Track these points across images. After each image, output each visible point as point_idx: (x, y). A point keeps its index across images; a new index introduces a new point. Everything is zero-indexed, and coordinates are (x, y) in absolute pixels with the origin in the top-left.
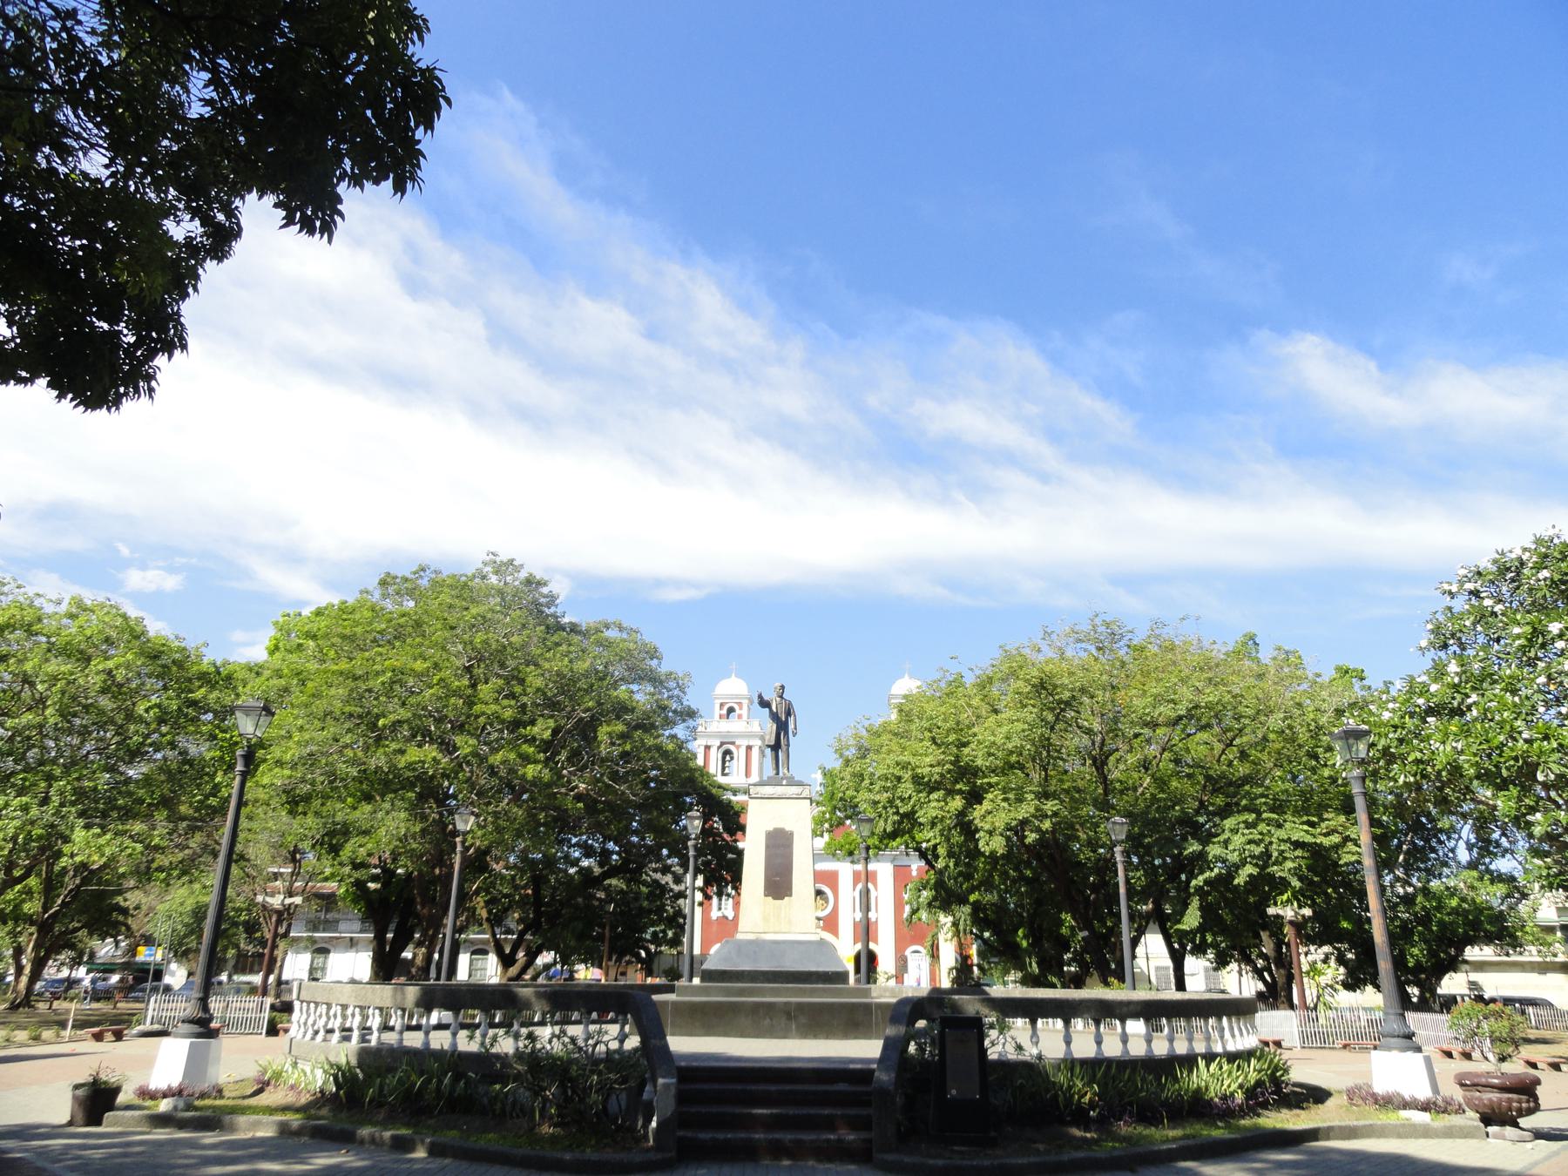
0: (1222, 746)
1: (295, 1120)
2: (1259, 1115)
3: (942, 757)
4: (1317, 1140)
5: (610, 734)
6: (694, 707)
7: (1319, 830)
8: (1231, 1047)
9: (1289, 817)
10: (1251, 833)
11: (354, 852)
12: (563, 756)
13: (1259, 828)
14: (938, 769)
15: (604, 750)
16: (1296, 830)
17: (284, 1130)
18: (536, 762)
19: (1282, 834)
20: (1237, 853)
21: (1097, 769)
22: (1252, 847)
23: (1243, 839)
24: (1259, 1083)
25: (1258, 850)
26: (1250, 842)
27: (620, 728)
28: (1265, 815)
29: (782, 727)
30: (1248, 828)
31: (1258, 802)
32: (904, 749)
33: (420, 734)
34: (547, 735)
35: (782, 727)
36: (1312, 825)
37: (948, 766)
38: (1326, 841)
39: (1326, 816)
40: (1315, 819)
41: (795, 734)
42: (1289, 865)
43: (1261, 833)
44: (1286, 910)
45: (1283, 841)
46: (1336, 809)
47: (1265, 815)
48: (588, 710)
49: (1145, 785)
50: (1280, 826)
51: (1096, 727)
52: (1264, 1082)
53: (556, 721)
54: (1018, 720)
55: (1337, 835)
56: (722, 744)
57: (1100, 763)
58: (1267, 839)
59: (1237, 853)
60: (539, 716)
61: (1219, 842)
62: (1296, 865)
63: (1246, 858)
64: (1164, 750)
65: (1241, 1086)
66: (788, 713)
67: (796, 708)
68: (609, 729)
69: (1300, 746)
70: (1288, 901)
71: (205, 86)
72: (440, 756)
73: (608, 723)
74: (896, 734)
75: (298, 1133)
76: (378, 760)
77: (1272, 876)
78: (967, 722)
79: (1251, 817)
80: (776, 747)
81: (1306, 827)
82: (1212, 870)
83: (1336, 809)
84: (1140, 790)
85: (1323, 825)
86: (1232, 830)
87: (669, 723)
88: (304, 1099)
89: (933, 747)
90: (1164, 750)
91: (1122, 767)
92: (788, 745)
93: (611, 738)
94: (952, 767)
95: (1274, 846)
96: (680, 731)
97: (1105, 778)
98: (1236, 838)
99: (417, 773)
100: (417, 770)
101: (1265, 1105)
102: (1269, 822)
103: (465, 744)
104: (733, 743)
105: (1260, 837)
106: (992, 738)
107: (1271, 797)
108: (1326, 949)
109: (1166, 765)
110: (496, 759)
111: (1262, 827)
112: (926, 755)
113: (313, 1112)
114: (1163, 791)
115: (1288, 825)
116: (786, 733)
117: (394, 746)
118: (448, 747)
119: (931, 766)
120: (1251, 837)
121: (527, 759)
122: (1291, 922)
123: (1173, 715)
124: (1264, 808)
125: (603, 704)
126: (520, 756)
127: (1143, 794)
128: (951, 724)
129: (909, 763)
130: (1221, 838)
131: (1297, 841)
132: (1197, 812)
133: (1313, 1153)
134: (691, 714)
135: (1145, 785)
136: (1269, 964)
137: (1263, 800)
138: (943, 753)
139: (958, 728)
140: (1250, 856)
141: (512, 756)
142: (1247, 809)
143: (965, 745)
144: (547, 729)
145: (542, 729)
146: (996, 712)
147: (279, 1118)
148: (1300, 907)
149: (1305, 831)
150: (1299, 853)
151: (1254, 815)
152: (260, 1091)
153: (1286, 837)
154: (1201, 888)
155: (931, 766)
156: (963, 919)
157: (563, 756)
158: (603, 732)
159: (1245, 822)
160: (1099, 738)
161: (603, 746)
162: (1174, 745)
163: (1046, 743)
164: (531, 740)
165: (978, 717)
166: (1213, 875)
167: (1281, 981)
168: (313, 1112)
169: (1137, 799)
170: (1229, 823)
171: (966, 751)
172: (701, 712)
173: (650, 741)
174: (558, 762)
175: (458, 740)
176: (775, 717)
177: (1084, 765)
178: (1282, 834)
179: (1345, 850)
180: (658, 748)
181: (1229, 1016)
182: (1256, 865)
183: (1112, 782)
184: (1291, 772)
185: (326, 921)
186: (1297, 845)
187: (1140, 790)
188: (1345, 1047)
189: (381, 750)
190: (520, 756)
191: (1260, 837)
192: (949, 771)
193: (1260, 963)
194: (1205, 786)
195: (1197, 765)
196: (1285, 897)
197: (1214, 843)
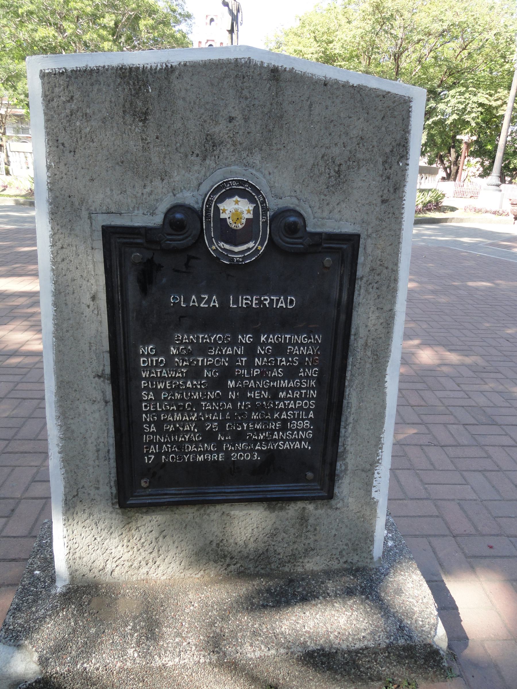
0: (460, 50)
1: (22, 200)
2: (426, 214)
3: (319, 48)
4: (446, 222)
5: (145, 25)
6: (190, 12)
7: (493, 98)
8: (423, 187)
9: (481, 90)
10: (461, 98)
11: (23, 88)
12: (123, 39)
13: (465, 96)
14: (315, 56)
15: (144, 35)
16: (482, 97)
17: (17, 203)
18: (109, 40)
19: (475, 99)
20: (451, 108)
21: (395, 61)
22: (459, 105)
23: (456, 101)
24: (430, 202)
25: (461, 107)
26: (459, 103)
27: (151, 22)
28: (470, 89)
29: (235, 19)
30: (460, 95)
31: (469, 81)
32: (300, 43)
33: (44, 21)
34: (112, 24)
35: (235, 19)
36: (491, 95)
37: (321, 54)
38: (494, 104)
39: (499, 90)
40: (493, 92)
41: (241, 24)
42: (473, 115)
43: (465, 98)
44: (465, 137)
45: (475, 103)
46: (505, 87)
47: (470, 89)
48: (133, 10)
49: (417, 71)
50: (475, 95)
51: (400, 35)
52: (432, 201)
53: (116, 17)
54: (361, 28)
55: (500, 101)
56: (208, 41)
57: (397, 57)
58: (467, 101)
59: (451, 108)
60: (107, 12)
61: (444, 102)
62: (476, 115)
63: (454, 111)
64: (431, 51)
65: (422, 202)
66: (238, 11)
67: (243, 8)
68: (145, 23)
69: (499, 51)
70: (468, 133)
71: (319, 599)
72: (56, 34)
73: (145, 19)
74: (296, 34)
75: (23, 204)
76: (23, 35)
77: (464, 120)
78: (334, 28)
79: (463, 89)
80: (231, 31)
81: (487, 96)
82: (437, 116)
83: (505, 87)
84: (414, 73)
85: (496, 95)
86: (452, 96)
87: (178, 22)
88: (24, 193)
89: (315, 42)
90: (431, 51)
91: (408, 61)
92: (238, 31)
93: (147, 28)
94: (323, 55)
95: (470, 105)
96: (183, 27)
97: (398, 67)
98: (453, 100)
99: (46, 44)
100: (46, 42)
101: (429, 210)
102: (471, 92)
103: (69, 27)
104: (213, 41)
105: (464, 100)
106: (346, 38)
107: (476, 79)
108: (478, 159)
109: (429, 60)
110: (87, 37)
111: (467, 95)
112: (310, 47)
113: (28, 197)
114: (425, 74)
115: (479, 95)
116: (237, 23)
117: (30, 27)
118: (61, 30)
119: (312, 53)
120: (460, 100)
121: (103, 39)
122: (466, 143)
123: (441, 29)
124: (471, 85)
125: (140, 6)
126: (99, 36)
127: (415, 75)
128: (325, 29)
129: (301, 51)
130: (446, 100)
131: (481, 103)
132: (439, 86)
133: (443, 226)
134: (188, 16)
135: (417, 71)
136: (451, 165)
137: (472, 80)
138: (319, 46)
139: (328, 32)
140: (457, 110)
141: (95, 36)
142: (463, 85)
143: (331, 42)
144: (111, 20)
145: (109, 20)
146: (349, 22)
147: (15, 198)
148: (472, 136)
149: (487, 98)
150: (480, 109)
151: (465, 89)
152: (4, 190)
153: (476, 101)
154: (430, 125)
155: (312, 53)
156: (361, 297)
157: (123, 39)
158: (142, 23)
159: (460, 92)
160: (399, 42)
161: (143, 33)
162: (437, 48)
163: (373, 44)
164: (105, 27)
165: (340, 25)
166: (437, 119)
167: (454, 171)
168: (28, 197)
169: (411, 78)
170: (452, 92)
171: (331, 45)
172: (194, 16)
173: (168, 32)
174: (120, 43)
175: (65, 24)
176: (231, 12)
177: (390, 58)
178: (475, 99)
179: (502, 109)
180: (172, 36)
181: (425, 174)
182: (458, 114)
183: (401, 69)
184: (490, 68)
185: (23, 129)
186: (481, 105)
187: (414, 73)
188: (471, 197)
189: (24, 29)
190: (99, 36)
191: (464, 100)
192: (321, 57)
193: (447, 164)
194: (446, 72)
195: (446, 60)
196: (466, 131)
197: (442, 103)
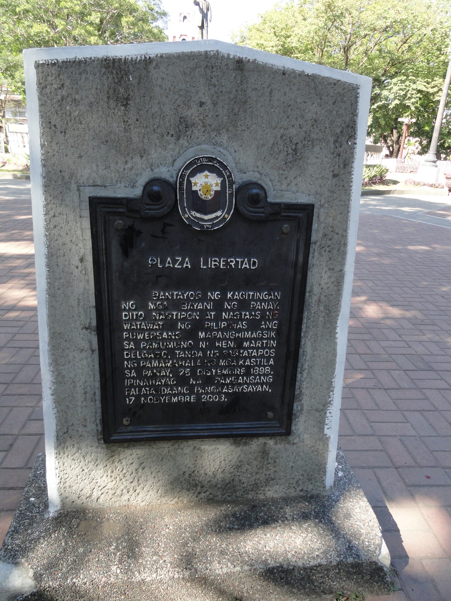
0: (401, 43)
1: (19, 174)
2: (372, 186)
3: (278, 42)
4: (389, 194)
5: (127, 22)
6: (166, 11)
7: (430, 85)
8: (369, 163)
9: (420, 79)
10: (402, 85)
11: (20, 76)
12: (107, 34)
13: (406, 83)
14: (275, 49)
15: (126, 31)
16: (421, 85)
17: (15, 177)
18: (95, 35)
19: (414, 86)
20: (394, 94)
21: (345, 53)
22: (401, 92)
23: (398, 88)
24: (375, 176)
25: (402, 93)
26: (400, 90)
27: (132, 19)
28: (410, 78)
29: (205, 16)
30: (401, 83)
31: (409, 71)
32: (261, 37)
33: (38, 18)
34: (98, 21)
35: (205, 16)
36: (428, 83)
37: (280, 47)
38: (431, 91)
39: (435, 79)
40: (430, 80)
41: (211, 21)
42: (413, 100)
43: (406, 86)
44: (405, 120)
45: (414, 89)
46: (440, 76)
47: (410, 78)
48: (116, 9)
49: (364, 62)
50: (414, 83)
51: (349, 31)
52: (377, 176)
53: (102, 14)
54: (315, 24)
55: (436, 88)
56: (181, 35)
57: (346, 50)
58: (408, 88)
59: (394, 94)
60: (93, 11)
61: (387, 89)
62: (416, 100)
63: (396, 97)
64: (376, 44)
65: (368, 176)
66: (208, 9)
67: (212, 7)
68: (127, 20)
69: (435, 44)
70: (408, 116)
71: (279, 523)
72: (49, 30)
73: (126, 16)
74: (258, 30)
75: (20, 178)
76: (20, 30)
77: (405, 105)
78: (291, 25)
79: (404, 78)
80: (202, 27)
81: (425, 84)
82: (381, 101)
83: (440, 76)
84: (361, 64)
85: (433, 83)
86: (394, 84)
87: (155, 19)
88: (21, 168)
89: (275, 37)
90: (376, 44)
91: (356, 53)
92: (207, 27)
93: (128, 24)
94: (281, 48)
95: (410, 92)
96: (160, 23)
97: (347, 58)
98: (395, 87)
99: (40, 38)
100: (40, 37)
101: (375, 183)
102: (411, 81)
103: (60, 24)
104: (186, 35)
105: (405, 87)
106: (301, 34)
107: (415, 69)
108: (417, 139)
109: (375, 52)
110: (76, 32)
111: (407, 83)
112: (271, 41)
113: (25, 172)
114: (370, 64)
115: (418, 83)
116: (207, 20)
117: (26, 23)
118: (53, 26)
119: (272, 47)
120: (401, 87)
121: (90, 34)
122: (406, 124)
123: (384, 26)
124: (411, 74)
125: (122, 5)
126: (86, 31)
127: (362, 66)
128: (284, 26)
129: (263, 45)
130: (389, 87)
131: (419, 90)
132: (383, 75)
133: (386, 197)
134: (164, 14)
135: (364, 62)
136: (393, 144)
137: (411, 70)
138: (279, 40)
139: (287, 28)
140: (398, 96)
141: (83, 31)
142: (404, 74)
143: (289, 37)
144: (97, 18)
145: (95, 18)
146: (305, 19)
147: (13, 173)
148: (411, 118)
149: (424, 85)
150: (419, 95)
151: (405, 77)
152: (4, 166)
153: (415, 88)
154: (375, 109)
155: (272, 47)
156: (315, 259)
157: (107, 34)
158: (124, 20)
159: (401, 80)
160: (348, 37)
161: (125, 29)
162: (381, 42)
163: (325, 38)
164: (91, 24)
165: (296, 22)
166: (381, 103)
167: (396, 149)
168: (25, 172)
169: (359, 68)
170: (395, 80)
171: (289, 40)
172: (169, 14)
173: (146, 28)
174: (105, 38)
175: (57, 21)
176: (201, 10)
177: (340, 51)
178: (414, 86)
179: (438, 95)
180: (150, 31)
181: (371, 151)
182: (399, 100)
183: (350, 60)
184: (428, 59)
185: (20, 112)
186: (420, 91)
187: (361, 64)
188: (411, 172)
189: (21, 25)
190: (86, 31)
191: (405, 87)
192: (280, 50)
193: (390, 143)
194: (389, 63)
195: (389, 52)
196: (407, 114)
197: (385, 89)
